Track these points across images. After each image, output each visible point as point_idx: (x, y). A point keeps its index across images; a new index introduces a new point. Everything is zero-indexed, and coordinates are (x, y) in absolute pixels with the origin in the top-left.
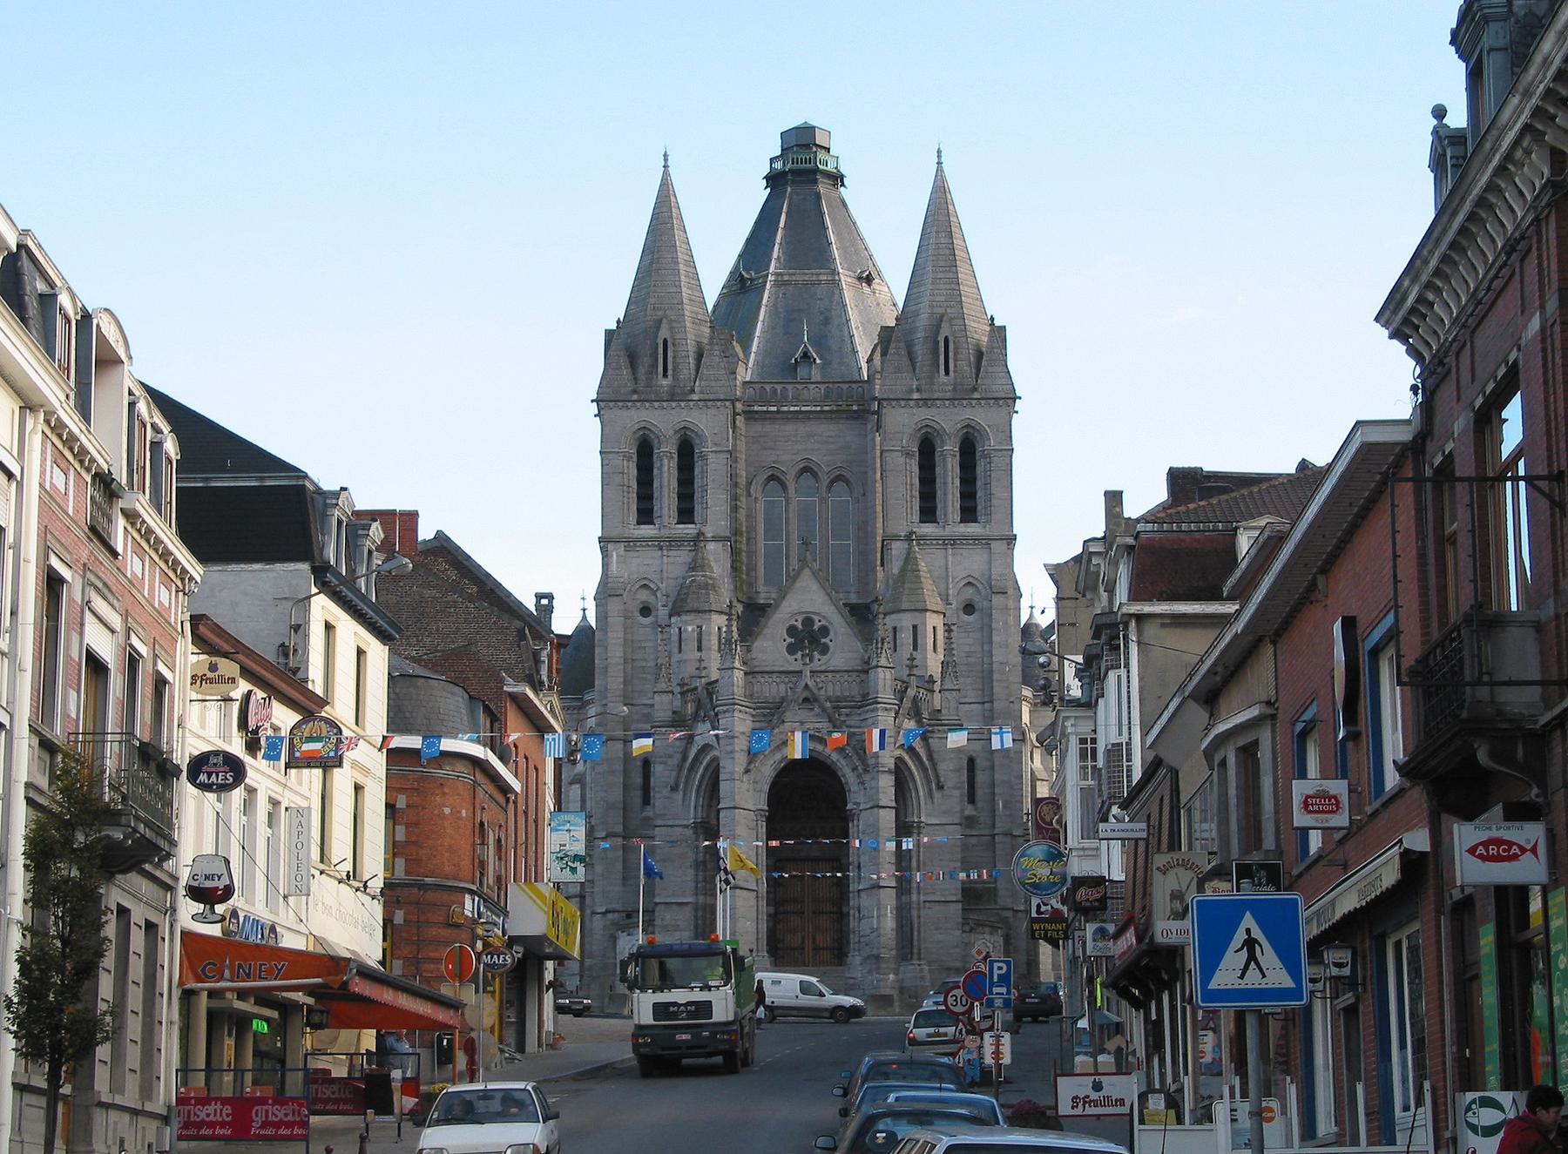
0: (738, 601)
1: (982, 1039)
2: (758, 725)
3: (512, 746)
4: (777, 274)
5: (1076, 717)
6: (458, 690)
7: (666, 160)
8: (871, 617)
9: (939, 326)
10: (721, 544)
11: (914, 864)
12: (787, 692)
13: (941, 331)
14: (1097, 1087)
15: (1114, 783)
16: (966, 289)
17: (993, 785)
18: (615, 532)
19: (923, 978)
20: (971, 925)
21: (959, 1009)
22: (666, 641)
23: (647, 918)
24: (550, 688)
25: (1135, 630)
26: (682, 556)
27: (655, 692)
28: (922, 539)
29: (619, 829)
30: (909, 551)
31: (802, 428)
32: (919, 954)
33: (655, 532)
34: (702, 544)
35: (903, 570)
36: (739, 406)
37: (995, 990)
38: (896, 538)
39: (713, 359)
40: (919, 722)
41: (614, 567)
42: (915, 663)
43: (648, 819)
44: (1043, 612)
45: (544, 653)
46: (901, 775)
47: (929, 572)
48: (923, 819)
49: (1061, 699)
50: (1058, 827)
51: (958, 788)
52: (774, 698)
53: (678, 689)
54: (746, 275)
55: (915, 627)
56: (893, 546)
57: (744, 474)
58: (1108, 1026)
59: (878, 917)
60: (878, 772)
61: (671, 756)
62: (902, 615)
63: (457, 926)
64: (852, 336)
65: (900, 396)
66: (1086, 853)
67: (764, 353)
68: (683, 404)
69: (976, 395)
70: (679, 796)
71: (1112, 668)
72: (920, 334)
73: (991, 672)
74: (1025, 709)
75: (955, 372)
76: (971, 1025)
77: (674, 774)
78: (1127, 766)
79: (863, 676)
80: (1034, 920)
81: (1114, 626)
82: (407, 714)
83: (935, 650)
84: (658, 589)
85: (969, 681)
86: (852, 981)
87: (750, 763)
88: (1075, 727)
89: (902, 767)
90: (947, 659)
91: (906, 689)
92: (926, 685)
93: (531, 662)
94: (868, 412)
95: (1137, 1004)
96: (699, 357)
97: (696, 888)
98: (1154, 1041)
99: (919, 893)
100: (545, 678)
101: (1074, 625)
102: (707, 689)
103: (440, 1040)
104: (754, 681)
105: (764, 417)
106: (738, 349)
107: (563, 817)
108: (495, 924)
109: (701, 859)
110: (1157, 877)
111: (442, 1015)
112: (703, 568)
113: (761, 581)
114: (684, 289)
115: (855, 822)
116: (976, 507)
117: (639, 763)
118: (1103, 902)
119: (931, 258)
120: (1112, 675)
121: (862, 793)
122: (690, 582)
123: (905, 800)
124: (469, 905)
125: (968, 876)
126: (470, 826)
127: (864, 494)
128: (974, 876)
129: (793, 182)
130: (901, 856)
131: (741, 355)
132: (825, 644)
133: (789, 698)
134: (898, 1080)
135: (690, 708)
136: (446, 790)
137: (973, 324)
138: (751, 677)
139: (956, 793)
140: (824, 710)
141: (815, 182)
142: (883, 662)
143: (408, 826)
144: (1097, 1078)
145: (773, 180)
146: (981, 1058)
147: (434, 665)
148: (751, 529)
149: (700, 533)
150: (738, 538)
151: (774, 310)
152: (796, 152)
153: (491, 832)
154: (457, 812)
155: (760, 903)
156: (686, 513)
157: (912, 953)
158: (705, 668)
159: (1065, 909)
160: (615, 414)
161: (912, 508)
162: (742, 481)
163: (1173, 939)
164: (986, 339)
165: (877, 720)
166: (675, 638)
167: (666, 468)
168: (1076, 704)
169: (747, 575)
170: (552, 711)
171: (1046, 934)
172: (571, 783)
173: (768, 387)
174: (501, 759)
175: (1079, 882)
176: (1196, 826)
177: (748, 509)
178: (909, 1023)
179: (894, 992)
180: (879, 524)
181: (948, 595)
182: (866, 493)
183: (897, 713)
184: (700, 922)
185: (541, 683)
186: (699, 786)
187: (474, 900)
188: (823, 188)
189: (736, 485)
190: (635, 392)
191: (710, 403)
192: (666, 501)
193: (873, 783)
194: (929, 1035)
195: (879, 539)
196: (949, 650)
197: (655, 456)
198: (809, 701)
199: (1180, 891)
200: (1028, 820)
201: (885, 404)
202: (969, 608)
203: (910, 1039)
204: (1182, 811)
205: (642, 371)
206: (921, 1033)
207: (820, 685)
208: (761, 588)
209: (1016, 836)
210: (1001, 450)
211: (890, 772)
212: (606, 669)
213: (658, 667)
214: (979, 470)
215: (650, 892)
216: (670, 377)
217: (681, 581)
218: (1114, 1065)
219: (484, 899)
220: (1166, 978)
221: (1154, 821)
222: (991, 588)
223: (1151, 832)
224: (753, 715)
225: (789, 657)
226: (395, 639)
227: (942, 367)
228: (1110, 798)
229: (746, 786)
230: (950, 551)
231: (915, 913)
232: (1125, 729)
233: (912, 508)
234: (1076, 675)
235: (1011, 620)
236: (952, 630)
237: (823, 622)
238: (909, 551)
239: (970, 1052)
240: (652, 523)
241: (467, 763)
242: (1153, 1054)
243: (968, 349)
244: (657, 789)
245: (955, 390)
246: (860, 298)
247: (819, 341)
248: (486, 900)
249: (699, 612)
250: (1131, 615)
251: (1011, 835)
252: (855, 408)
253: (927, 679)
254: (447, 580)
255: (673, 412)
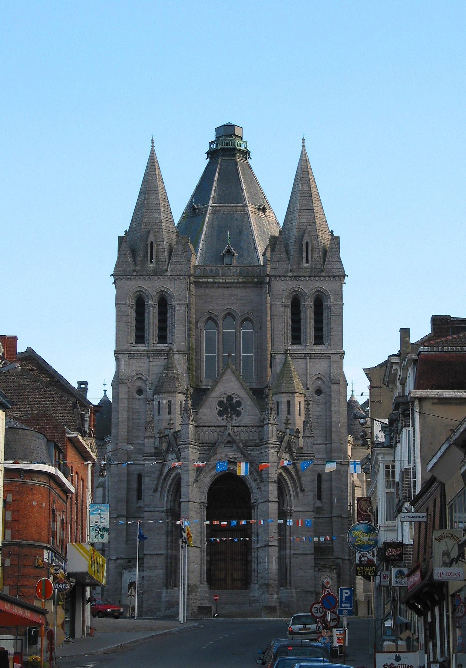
0: (191, 387)
1: (332, 632)
2: (202, 456)
3: (70, 467)
4: (213, 206)
5: (383, 453)
6: (41, 436)
7: (153, 143)
8: (264, 396)
9: (303, 236)
10: (181, 355)
11: (288, 533)
12: (218, 437)
13: (304, 238)
14: (398, 659)
15: (406, 490)
16: (318, 215)
17: (331, 490)
18: (124, 348)
19: (292, 597)
20: (319, 567)
21: (319, 615)
22: (151, 409)
23: (140, 562)
24: (90, 435)
25: (418, 406)
26: (160, 362)
27: (145, 437)
28: (293, 353)
29: (124, 512)
30: (286, 360)
31: (227, 292)
32: (290, 583)
33: (146, 348)
34: (171, 355)
35: (282, 370)
36: (192, 279)
37: (344, 605)
38: (279, 353)
39: (178, 253)
40: (291, 454)
41: (122, 367)
42: (289, 422)
43: (140, 507)
44: (362, 394)
45: (87, 415)
46: (281, 484)
47: (297, 371)
48: (293, 508)
49: (373, 443)
50: (370, 514)
51: (313, 491)
52: (211, 440)
53: (157, 435)
54: (196, 207)
55: (289, 402)
56: (277, 357)
57: (194, 316)
58: (400, 625)
59: (268, 562)
60: (268, 482)
61: (154, 473)
62: (283, 395)
63: (40, 567)
64: (254, 241)
65: (281, 275)
66: (389, 528)
67: (206, 250)
68: (161, 278)
69: (323, 274)
70: (158, 495)
71: (405, 426)
72: (292, 240)
73: (331, 427)
74: (349, 448)
75: (312, 261)
76: (325, 624)
77: (155, 482)
78: (414, 481)
79: (260, 429)
80: (357, 565)
81: (406, 403)
82: (13, 450)
83: (300, 415)
84: (147, 380)
85: (318, 432)
86: (253, 598)
87: (197, 476)
88: (383, 459)
89: (282, 479)
90: (307, 419)
91: (284, 436)
92: (295, 434)
93: (80, 421)
94: (263, 282)
95: (420, 613)
96: (171, 251)
97: (167, 546)
98: (430, 633)
99: (290, 549)
100: (87, 429)
101: (379, 402)
102: (174, 436)
103: (30, 631)
104: (200, 431)
105: (206, 285)
106: (191, 247)
107: (97, 507)
108: (61, 566)
109: (170, 530)
110: (435, 543)
111: (36, 618)
112: (172, 368)
113: (203, 375)
114: (162, 214)
115: (256, 510)
116: (323, 336)
117: (136, 476)
118: (401, 557)
119: (299, 198)
120: (405, 431)
121: (259, 493)
122: (165, 376)
123: (283, 497)
124: (46, 556)
125: (319, 540)
126: (47, 512)
127: (261, 328)
128: (322, 539)
129: (223, 155)
130: (281, 528)
131: (193, 251)
132: (239, 411)
133: (220, 441)
134: (292, 655)
135: (164, 446)
136: (34, 492)
137: (321, 235)
138: (198, 429)
139: (311, 494)
140: (238, 447)
141: (234, 155)
142: (272, 421)
143: (13, 511)
144: (398, 654)
145: (211, 154)
146: (331, 642)
147: (28, 422)
148: (198, 347)
149: (171, 349)
150: (191, 352)
151: (211, 224)
152: (224, 139)
153: (58, 515)
154: (39, 504)
155: (203, 554)
156: (162, 338)
157: (286, 583)
158: (173, 424)
159: (375, 559)
160: (122, 283)
161: (287, 336)
162: (193, 320)
163: (444, 578)
164: (328, 243)
165: (268, 453)
166: (156, 407)
167: (152, 313)
168: (381, 445)
169: (196, 372)
170: (91, 448)
171: (364, 573)
172: (97, 487)
173: (208, 269)
174: (64, 474)
175: (388, 545)
176: (455, 515)
177: (196, 336)
178: (289, 622)
179: (277, 604)
180: (269, 345)
181: (307, 384)
182: (262, 327)
183: (279, 449)
184: (169, 565)
185: (85, 432)
186: (169, 489)
187: (49, 553)
188: (239, 158)
189: (190, 322)
190: (135, 271)
191: (176, 277)
192: (151, 331)
193: (266, 488)
194: (300, 629)
195: (269, 353)
196: (307, 415)
197: (146, 306)
198: (230, 442)
199: (448, 551)
200: (351, 509)
201: (273, 278)
202: (319, 392)
203: (289, 631)
204: (447, 507)
205: (139, 259)
206: (296, 628)
207: (237, 434)
208: (204, 380)
209: (344, 518)
210: (337, 304)
211: (275, 482)
212: (117, 424)
213: (147, 423)
214: (325, 315)
215: (142, 548)
216: (154, 263)
217: (160, 375)
218: (405, 647)
219: (54, 553)
220: (437, 599)
221: (431, 511)
222: (331, 381)
223: (429, 518)
224: (199, 450)
225: (219, 418)
226: (9, 408)
227: (305, 259)
228: (403, 499)
229: (195, 489)
230: (308, 360)
231: (288, 560)
232: (412, 462)
233: (287, 336)
234: (382, 430)
235: (342, 398)
236: (309, 404)
237: (238, 399)
238: (286, 360)
239: (325, 639)
240: (144, 343)
241: (45, 476)
242: (429, 641)
243: (319, 249)
244: (145, 491)
245: (311, 271)
246: (259, 220)
247: (237, 244)
248: (55, 553)
249: (169, 392)
250: (416, 398)
251: (341, 517)
252: (256, 280)
253: (295, 430)
254: (33, 375)
255: (156, 282)
